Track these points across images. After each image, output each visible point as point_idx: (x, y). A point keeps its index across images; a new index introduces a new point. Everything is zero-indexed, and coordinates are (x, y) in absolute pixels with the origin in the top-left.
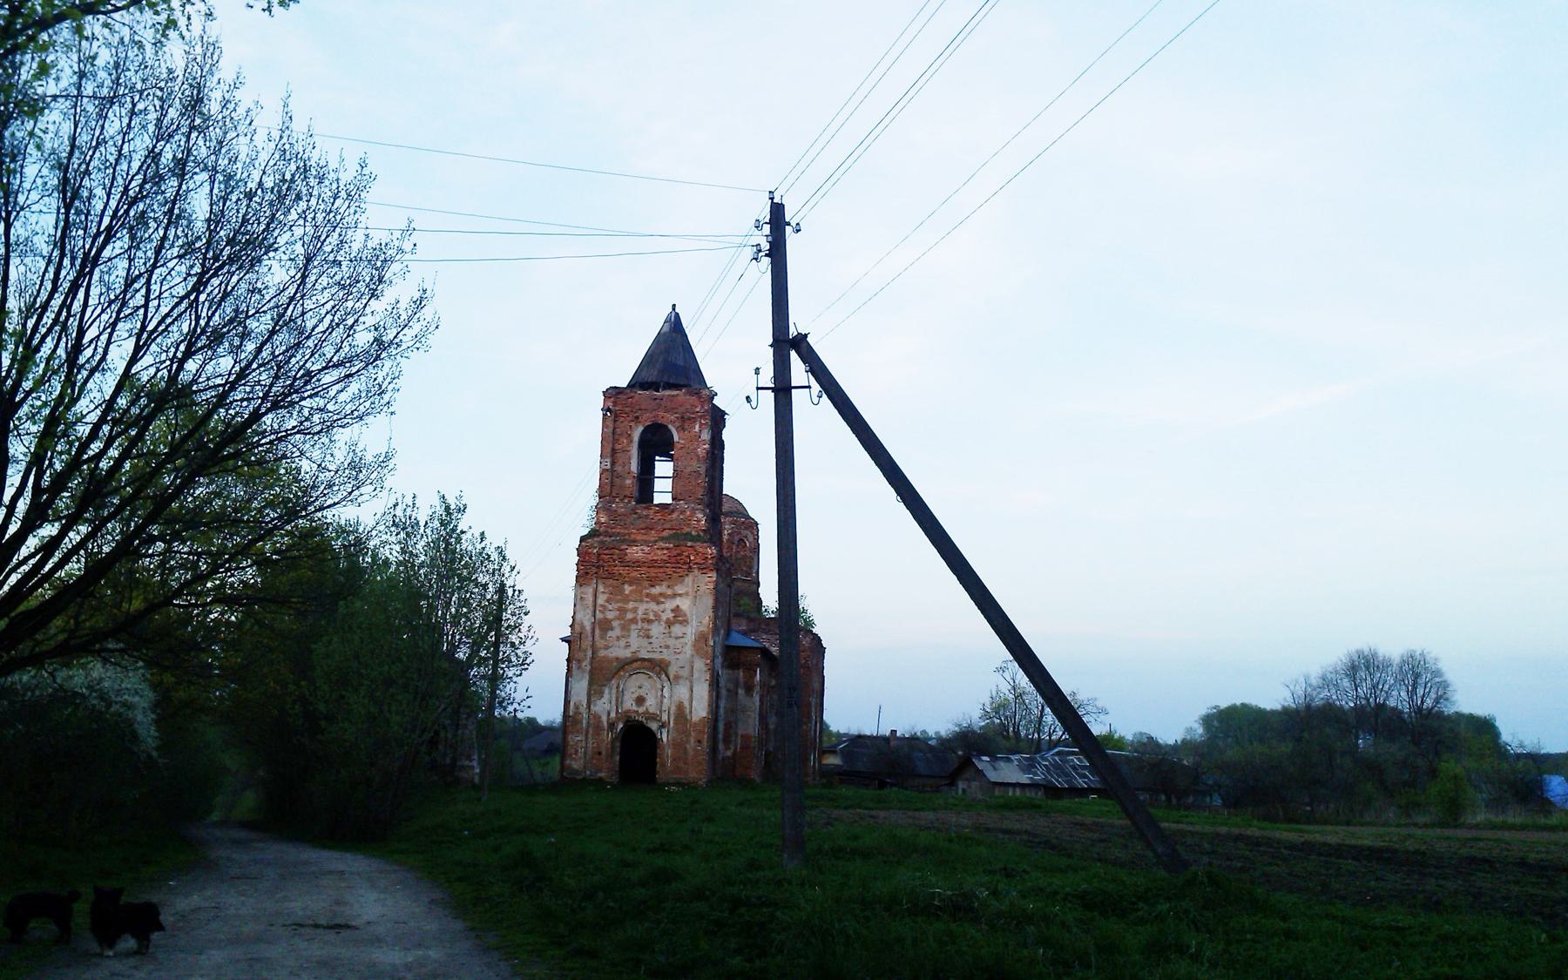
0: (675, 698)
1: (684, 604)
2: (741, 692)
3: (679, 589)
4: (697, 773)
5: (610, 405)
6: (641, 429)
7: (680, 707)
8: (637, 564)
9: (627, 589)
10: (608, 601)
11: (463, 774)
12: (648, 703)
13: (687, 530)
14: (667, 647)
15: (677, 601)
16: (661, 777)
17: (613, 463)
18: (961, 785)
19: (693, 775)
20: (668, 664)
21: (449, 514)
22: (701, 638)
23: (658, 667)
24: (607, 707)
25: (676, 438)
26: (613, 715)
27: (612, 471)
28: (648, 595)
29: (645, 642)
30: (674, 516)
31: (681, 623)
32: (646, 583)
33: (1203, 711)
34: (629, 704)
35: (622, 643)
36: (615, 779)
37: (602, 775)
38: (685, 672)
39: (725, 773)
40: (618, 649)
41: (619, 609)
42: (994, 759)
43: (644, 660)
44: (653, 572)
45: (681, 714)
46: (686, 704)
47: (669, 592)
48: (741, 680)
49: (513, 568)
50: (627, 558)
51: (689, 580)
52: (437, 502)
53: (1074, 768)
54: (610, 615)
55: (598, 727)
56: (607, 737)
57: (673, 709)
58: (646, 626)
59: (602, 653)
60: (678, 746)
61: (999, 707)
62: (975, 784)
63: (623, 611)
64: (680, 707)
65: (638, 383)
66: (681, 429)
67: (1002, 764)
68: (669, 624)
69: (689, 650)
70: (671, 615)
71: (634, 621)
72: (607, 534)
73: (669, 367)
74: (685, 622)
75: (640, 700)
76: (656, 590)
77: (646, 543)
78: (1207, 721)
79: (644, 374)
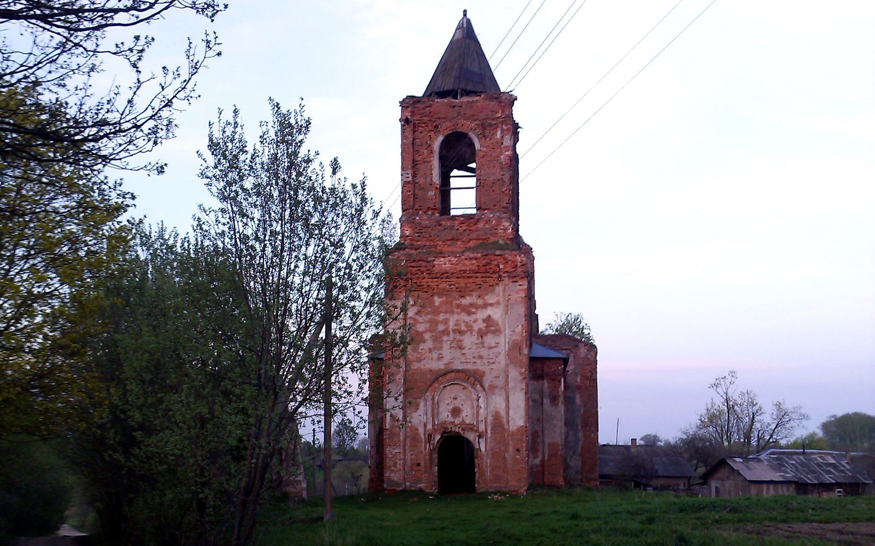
0: (492, 408)
1: (496, 313)
2: (546, 401)
3: (490, 299)
4: (518, 482)
5: (408, 115)
6: (441, 138)
7: (497, 416)
8: (445, 275)
9: (437, 300)
10: (418, 313)
11: (290, 489)
12: (464, 414)
13: (493, 239)
14: (481, 357)
15: (489, 311)
16: (480, 486)
17: (414, 175)
18: (714, 484)
19: (513, 484)
20: (483, 374)
21: (289, 130)
22: (515, 347)
23: (472, 378)
24: (423, 419)
25: (477, 146)
26: (430, 427)
27: (414, 183)
28: (458, 306)
29: (457, 353)
30: (480, 225)
31: (493, 332)
32: (456, 294)
33: (824, 419)
34: (445, 415)
35: (435, 355)
36: (434, 490)
37: (422, 485)
38: (500, 382)
39: (539, 481)
40: (430, 358)
41: (430, 321)
42: (746, 459)
43: (458, 371)
44: (462, 283)
45: (498, 424)
46: (503, 413)
47: (480, 302)
48: (546, 390)
49: (376, 214)
50: (436, 269)
51: (499, 289)
52: (269, 116)
53: (819, 465)
54: (421, 328)
55: (415, 439)
56: (425, 449)
57: (490, 419)
58: (458, 337)
59: (415, 366)
60: (497, 455)
61: (713, 418)
62: (729, 484)
63: (434, 323)
64: (497, 416)
65: (435, 90)
66: (482, 136)
67: (752, 463)
68: (482, 334)
69: (502, 360)
70: (483, 325)
71: (446, 332)
72: (411, 246)
73: (464, 74)
74: (497, 332)
75: (456, 412)
76: (467, 301)
77: (453, 254)
78: (825, 426)
79: (439, 83)
